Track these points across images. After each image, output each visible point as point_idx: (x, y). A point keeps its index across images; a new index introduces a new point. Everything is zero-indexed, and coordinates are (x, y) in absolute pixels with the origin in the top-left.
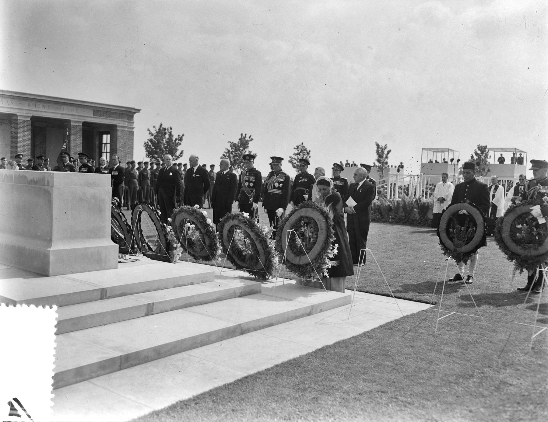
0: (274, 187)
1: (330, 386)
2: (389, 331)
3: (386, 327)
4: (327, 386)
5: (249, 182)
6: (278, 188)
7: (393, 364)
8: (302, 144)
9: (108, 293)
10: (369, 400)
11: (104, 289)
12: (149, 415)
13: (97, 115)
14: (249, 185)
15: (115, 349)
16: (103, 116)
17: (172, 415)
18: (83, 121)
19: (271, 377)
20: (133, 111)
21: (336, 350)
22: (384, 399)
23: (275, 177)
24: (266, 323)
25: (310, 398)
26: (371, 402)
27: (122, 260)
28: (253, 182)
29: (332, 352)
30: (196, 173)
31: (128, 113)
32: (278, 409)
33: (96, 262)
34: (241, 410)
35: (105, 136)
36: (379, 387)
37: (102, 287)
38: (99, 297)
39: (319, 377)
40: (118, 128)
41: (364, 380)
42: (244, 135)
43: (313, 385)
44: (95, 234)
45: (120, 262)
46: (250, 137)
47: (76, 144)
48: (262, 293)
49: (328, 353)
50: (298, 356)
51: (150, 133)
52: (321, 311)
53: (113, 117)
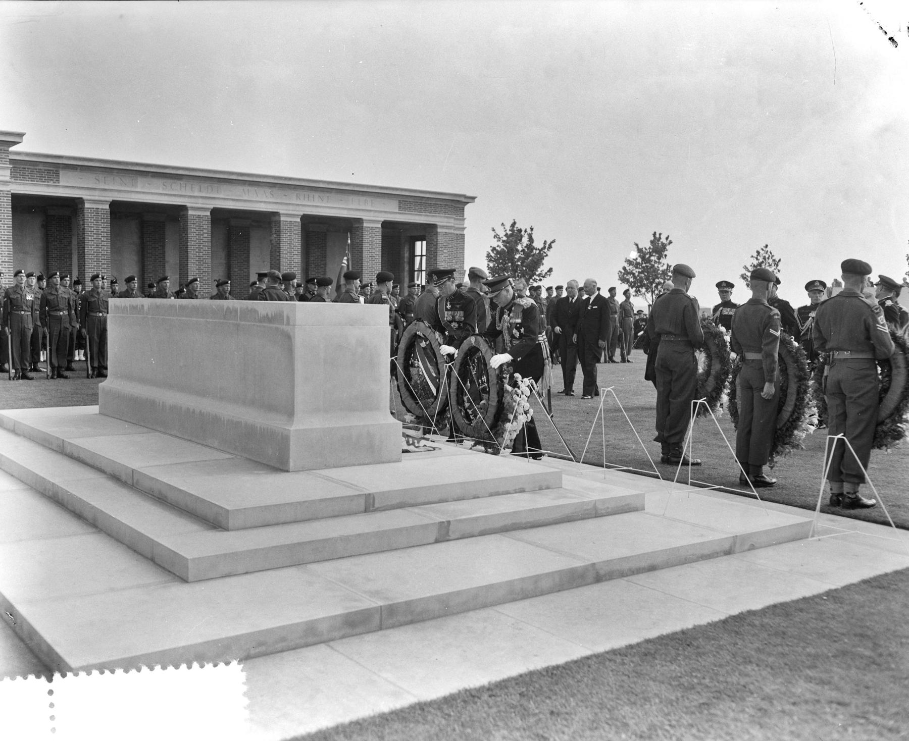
1: (739, 684)
2: (878, 591)
3: (874, 584)
4: (733, 684)
7: (872, 654)
8: (767, 246)
9: (376, 501)
10: (809, 717)
11: (370, 494)
12: (408, 708)
13: (405, 209)
15: (375, 594)
17: (447, 712)
19: (634, 659)
20: (463, 200)
21: (766, 620)
22: (841, 717)
24: (644, 564)
25: (695, 703)
26: (814, 720)
27: (411, 448)
29: (757, 623)
30: (593, 304)
31: (456, 204)
32: (633, 718)
33: (369, 451)
34: (567, 713)
35: (418, 244)
36: (834, 694)
37: (367, 492)
38: (363, 508)
39: (721, 666)
40: (439, 230)
41: (809, 679)
42: (658, 236)
43: (707, 681)
45: (405, 451)
46: (667, 238)
47: (291, 257)
48: (646, 510)
49: (749, 625)
50: (690, 626)
51: (496, 236)
52: (753, 548)
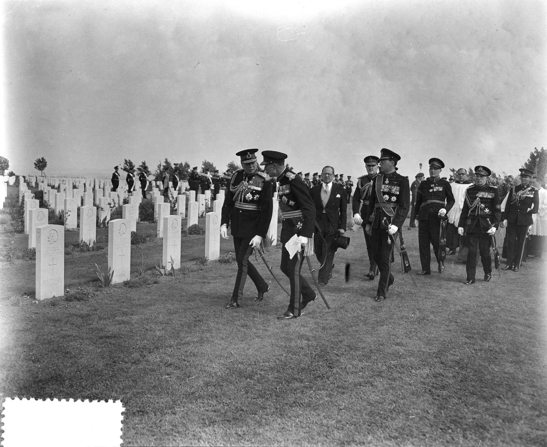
0: (245, 201)
5: (390, 194)
6: (252, 202)
14: (390, 199)
23: (245, 183)
28: (396, 195)
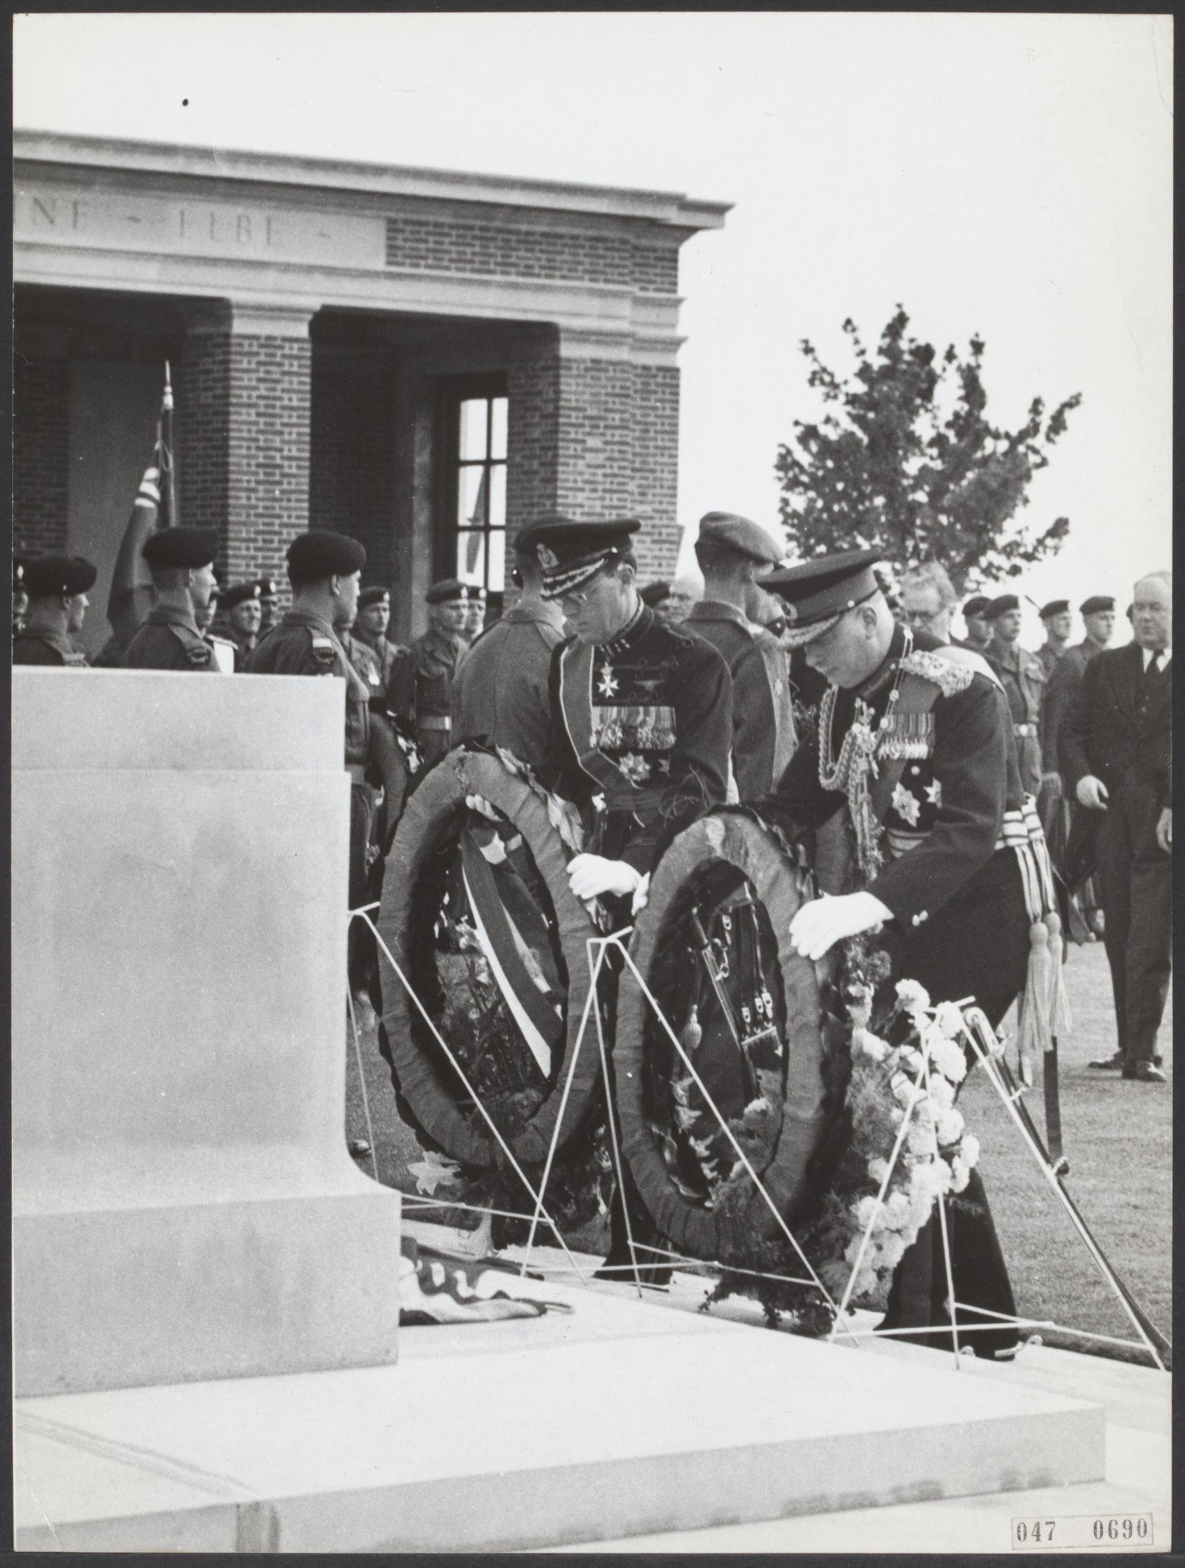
11: (256, 1507)
13: (415, 258)
16: (461, 261)
18: (316, 303)
20: (674, 216)
31: (641, 239)
35: (473, 411)
37: (245, 1497)
40: (567, 350)
44: (243, 1111)
45: (411, 1319)
53: (528, 272)
